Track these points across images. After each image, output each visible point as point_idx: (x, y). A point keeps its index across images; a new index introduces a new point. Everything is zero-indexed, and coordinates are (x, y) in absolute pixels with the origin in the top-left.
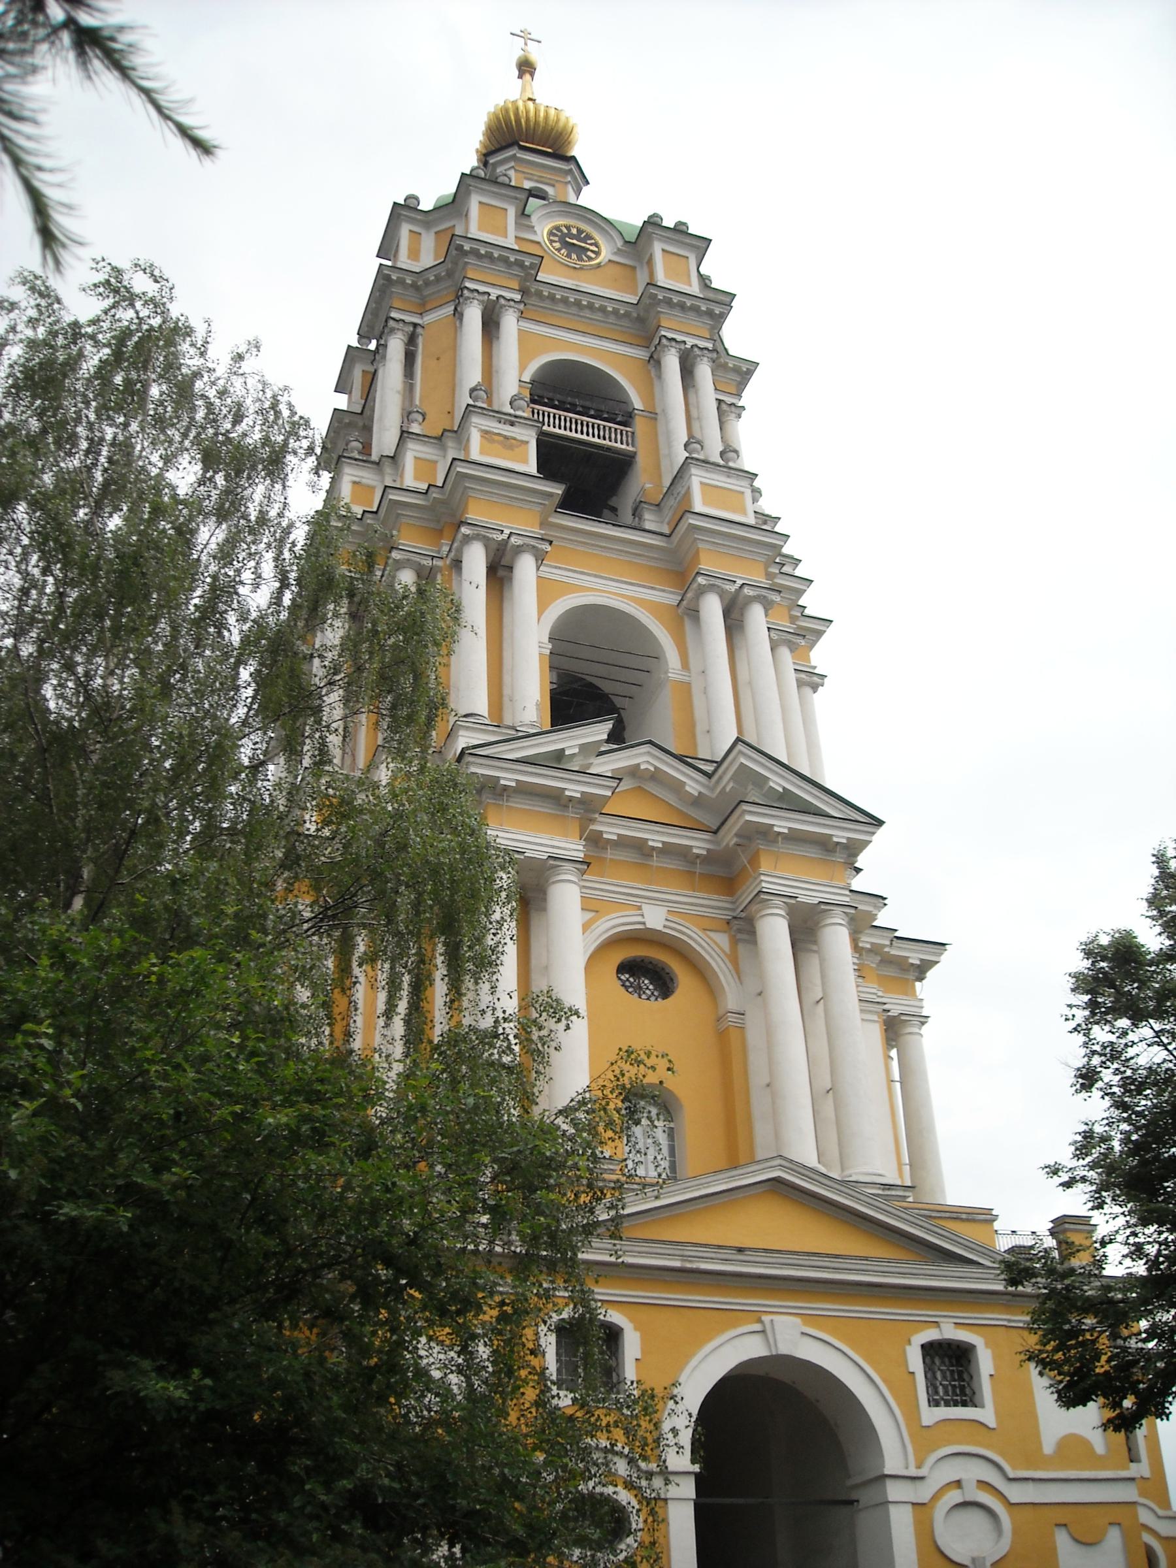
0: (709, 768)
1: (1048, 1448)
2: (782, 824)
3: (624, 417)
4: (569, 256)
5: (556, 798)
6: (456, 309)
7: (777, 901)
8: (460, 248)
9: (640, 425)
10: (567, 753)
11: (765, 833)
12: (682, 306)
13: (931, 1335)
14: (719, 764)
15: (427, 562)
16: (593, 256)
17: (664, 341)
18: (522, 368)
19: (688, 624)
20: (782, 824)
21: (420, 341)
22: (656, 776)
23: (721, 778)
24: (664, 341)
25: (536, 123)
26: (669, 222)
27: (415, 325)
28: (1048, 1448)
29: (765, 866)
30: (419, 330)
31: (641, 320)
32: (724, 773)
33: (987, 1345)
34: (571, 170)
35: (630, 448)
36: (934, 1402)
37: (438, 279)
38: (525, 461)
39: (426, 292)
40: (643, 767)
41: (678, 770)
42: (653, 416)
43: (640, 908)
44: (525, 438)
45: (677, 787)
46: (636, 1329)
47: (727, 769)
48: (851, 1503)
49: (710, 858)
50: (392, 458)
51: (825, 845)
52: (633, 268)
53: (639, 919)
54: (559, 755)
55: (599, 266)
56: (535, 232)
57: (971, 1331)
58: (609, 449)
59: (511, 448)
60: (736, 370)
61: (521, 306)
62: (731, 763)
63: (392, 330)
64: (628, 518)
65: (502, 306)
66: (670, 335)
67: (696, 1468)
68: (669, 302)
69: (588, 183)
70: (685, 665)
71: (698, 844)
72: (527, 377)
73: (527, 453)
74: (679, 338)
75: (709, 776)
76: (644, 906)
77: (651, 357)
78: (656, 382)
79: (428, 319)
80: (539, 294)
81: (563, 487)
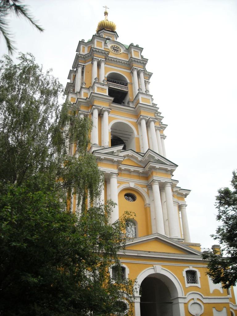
0: (143, 155)
1: (211, 292)
2: (158, 166)
3: (126, 84)
4: (115, 52)
5: (112, 161)
6: (92, 62)
7: (157, 181)
8: (93, 50)
9: (129, 86)
10: (114, 152)
11: (154, 168)
12: (137, 62)
13: (188, 269)
14: (145, 154)
15: (86, 113)
16: (119, 51)
17: (134, 69)
18: (105, 74)
19: (139, 126)
20: (158, 166)
21: (85, 69)
22: (132, 156)
23: (145, 157)
24: (134, 69)
25: (108, 25)
26: (135, 45)
27: (84, 66)
28: (211, 292)
29: (154, 174)
30: (84, 67)
31: (129, 65)
32: (146, 156)
33: (199, 271)
34: (115, 34)
35: (127, 90)
36: (188, 283)
37: (88, 56)
38: (106, 93)
39: (86, 59)
40: (130, 155)
41: (137, 155)
42: (132, 84)
43: (129, 183)
44: (106, 88)
45: (136, 159)
46: (128, 268)
47: (147, 154)
48: (172, 303)
49: (143, 173)
50: (79, 92)
51: (166, 170)
52: (128, 54)
53: (129, 185)
54: (113, 152)
55: (121, 54)
56: (108, 47)
57: (196, 268)
58: (123, 91)
59: (103, 90)
60: (148, 75)
61: (105, 62)
62: (147, 154)
63: (79, 67)
64: (126, 104)
65: (101, 62)
66: (135, 68)
67: (140, 296)
68: (135, 61)
69: (118, 37)
70: (138, 134)
71: (141, 170)
72: (106, 76)
73: (106, 91)
74: (137, 68)
75: (143, 156)
76: (130, 183)
77: (131, 72)
78: (132, 77)
79: (86, 64)
80: (109, 59)
81: (114, 98)
